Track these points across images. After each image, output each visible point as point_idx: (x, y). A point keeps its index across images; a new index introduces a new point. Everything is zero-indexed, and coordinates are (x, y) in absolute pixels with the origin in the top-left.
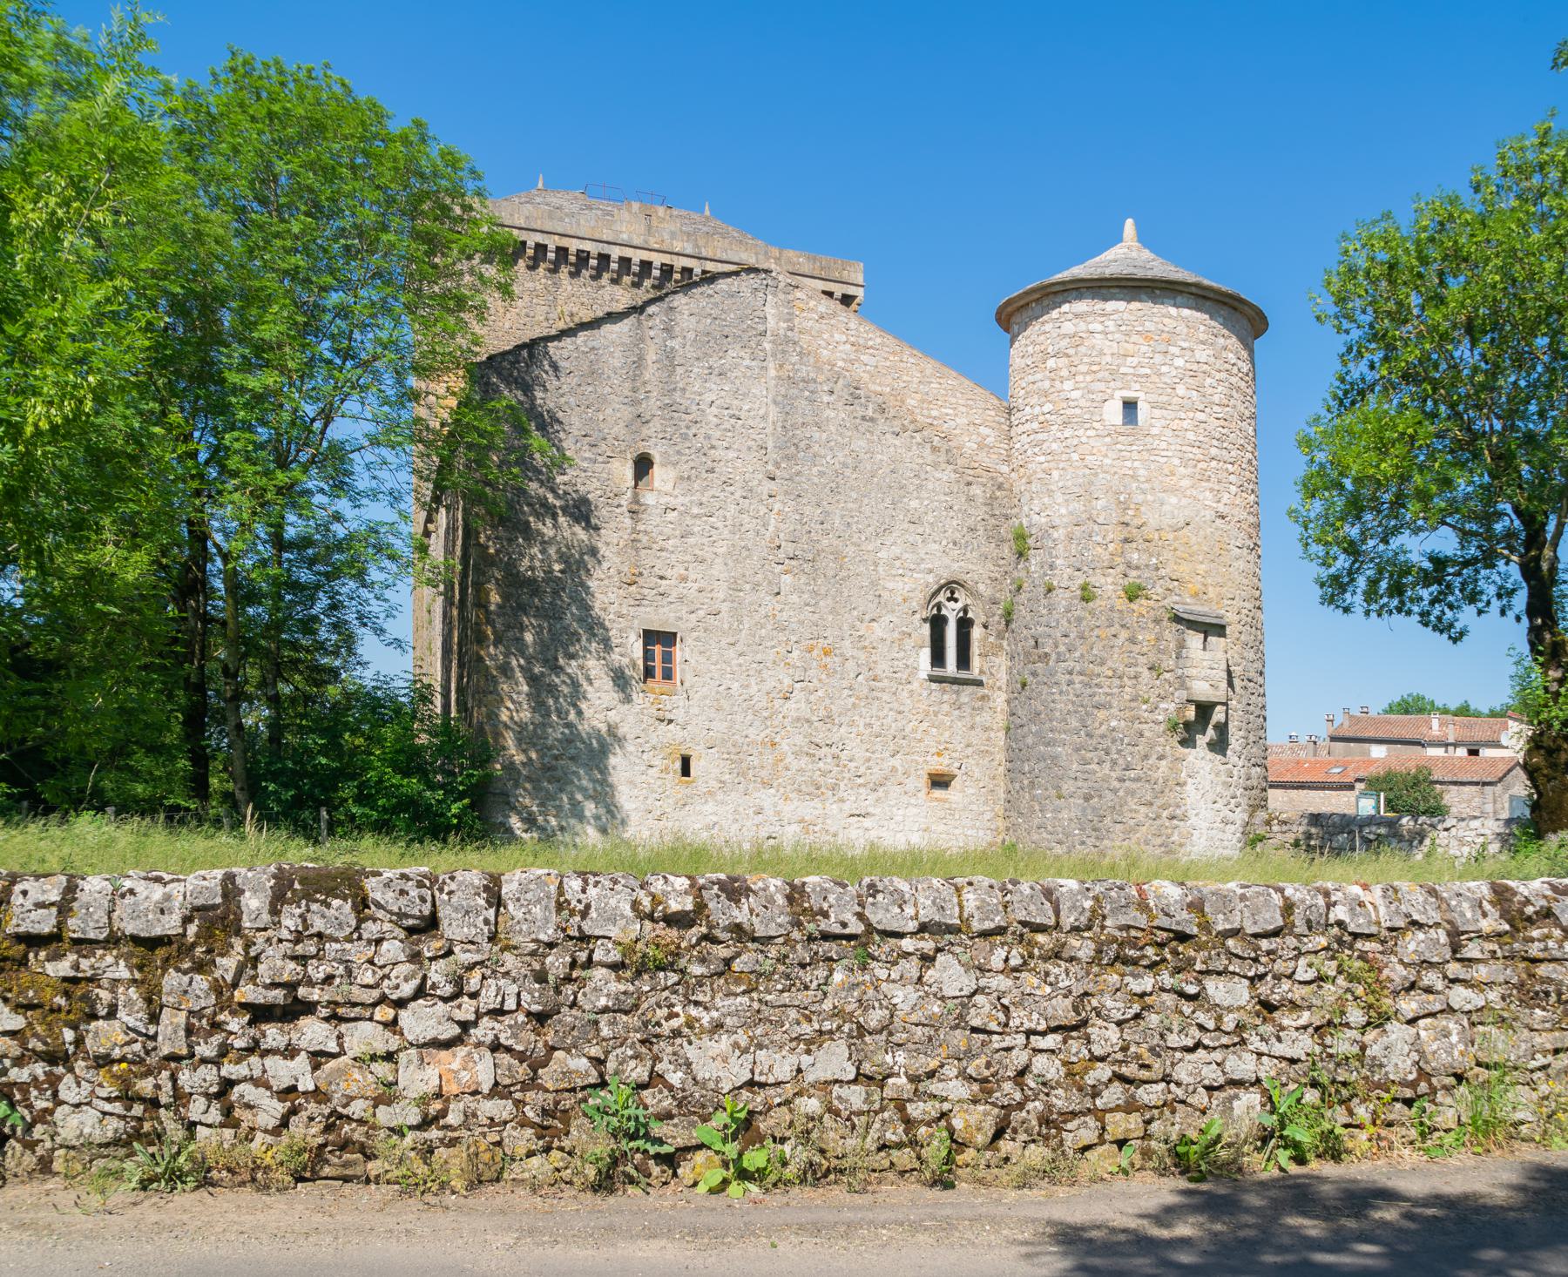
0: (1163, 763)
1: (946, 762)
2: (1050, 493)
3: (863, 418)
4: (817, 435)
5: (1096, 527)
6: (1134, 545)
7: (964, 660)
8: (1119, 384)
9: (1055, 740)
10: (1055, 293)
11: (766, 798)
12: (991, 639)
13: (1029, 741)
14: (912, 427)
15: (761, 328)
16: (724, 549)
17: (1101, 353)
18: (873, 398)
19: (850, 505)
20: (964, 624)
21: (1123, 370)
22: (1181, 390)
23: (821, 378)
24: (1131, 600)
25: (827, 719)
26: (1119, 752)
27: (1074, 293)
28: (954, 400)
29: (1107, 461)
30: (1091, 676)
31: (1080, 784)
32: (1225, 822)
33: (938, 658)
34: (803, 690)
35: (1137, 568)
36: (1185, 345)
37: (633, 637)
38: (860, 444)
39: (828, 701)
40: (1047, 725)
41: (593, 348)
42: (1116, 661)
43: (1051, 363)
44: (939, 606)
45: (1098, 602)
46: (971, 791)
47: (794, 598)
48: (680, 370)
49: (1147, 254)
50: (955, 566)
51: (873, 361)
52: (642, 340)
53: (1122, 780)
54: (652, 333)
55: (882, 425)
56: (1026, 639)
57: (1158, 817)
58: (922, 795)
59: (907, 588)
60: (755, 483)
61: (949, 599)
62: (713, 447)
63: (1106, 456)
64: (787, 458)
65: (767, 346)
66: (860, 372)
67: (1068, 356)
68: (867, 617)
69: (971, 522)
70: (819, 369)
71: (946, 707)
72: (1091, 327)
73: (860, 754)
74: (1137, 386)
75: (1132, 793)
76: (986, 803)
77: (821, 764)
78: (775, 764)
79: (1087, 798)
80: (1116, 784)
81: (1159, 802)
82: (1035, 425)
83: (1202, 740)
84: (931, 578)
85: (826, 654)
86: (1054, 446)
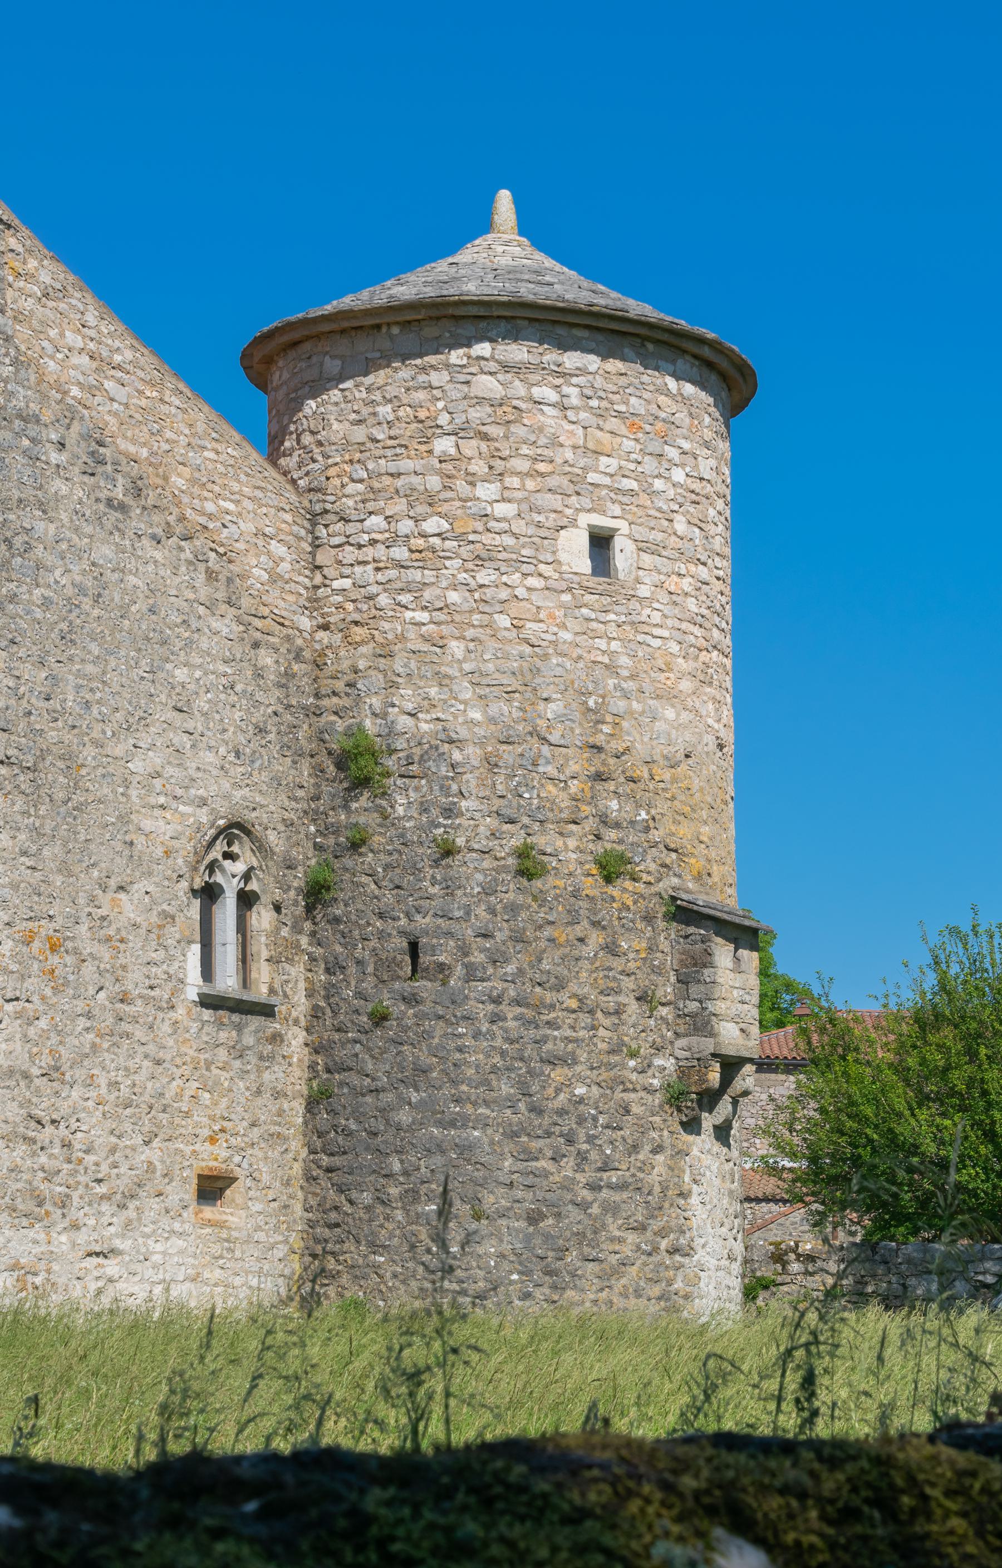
0: (660, 1158)
1: (224, 1154)
2: (442, 680)
4: (40, 526)
5: (545, 749)
6: (611, 786)
12: (285, 932)
13: (404, 1117)
14: (178, 530)
17: (555, 443)
19: (90, 669)
21: (592, 477)
22: (680, 526)
23: (47, 417)
24: (608, 879)
25: (53, 1073)
26: (590, 1139)
28: (236, 487)
29: (567, 636)
30: (539, 1007)
31: (519, 1194)
33: (207, 971)
34: (18, 1015)
35: (617, 825)
36: (686, 445)
38: (104, 552)
39: (54, 1039)
42: (583, 984)
43: (444, 445)
45: (551, 880)
46: (257, 1207)
50: (238, 794)
53: (594, 1187)
55: (136, 522)
56: (382, 936)
57: (656, 1249)
59: (170, 830)
61: (228, 856)
63: (563, 626)
66: (106, 414)
67: (485, 437)
68: (113, 883)
69: (257, 717)
70: (45, 397)
71: (222, 1054)
72: (537, 392)
73: (103, 1140)
74: (617, 510)
75: (612, 1209)
76: (276, 1229)
77: (43, 1159)
79: (534, 1218)
80: (586, 1194)
81: (655, 1225)
82: (400, 553)
83: (708, 1121)
85: (53, 949)
86: (453, 597)
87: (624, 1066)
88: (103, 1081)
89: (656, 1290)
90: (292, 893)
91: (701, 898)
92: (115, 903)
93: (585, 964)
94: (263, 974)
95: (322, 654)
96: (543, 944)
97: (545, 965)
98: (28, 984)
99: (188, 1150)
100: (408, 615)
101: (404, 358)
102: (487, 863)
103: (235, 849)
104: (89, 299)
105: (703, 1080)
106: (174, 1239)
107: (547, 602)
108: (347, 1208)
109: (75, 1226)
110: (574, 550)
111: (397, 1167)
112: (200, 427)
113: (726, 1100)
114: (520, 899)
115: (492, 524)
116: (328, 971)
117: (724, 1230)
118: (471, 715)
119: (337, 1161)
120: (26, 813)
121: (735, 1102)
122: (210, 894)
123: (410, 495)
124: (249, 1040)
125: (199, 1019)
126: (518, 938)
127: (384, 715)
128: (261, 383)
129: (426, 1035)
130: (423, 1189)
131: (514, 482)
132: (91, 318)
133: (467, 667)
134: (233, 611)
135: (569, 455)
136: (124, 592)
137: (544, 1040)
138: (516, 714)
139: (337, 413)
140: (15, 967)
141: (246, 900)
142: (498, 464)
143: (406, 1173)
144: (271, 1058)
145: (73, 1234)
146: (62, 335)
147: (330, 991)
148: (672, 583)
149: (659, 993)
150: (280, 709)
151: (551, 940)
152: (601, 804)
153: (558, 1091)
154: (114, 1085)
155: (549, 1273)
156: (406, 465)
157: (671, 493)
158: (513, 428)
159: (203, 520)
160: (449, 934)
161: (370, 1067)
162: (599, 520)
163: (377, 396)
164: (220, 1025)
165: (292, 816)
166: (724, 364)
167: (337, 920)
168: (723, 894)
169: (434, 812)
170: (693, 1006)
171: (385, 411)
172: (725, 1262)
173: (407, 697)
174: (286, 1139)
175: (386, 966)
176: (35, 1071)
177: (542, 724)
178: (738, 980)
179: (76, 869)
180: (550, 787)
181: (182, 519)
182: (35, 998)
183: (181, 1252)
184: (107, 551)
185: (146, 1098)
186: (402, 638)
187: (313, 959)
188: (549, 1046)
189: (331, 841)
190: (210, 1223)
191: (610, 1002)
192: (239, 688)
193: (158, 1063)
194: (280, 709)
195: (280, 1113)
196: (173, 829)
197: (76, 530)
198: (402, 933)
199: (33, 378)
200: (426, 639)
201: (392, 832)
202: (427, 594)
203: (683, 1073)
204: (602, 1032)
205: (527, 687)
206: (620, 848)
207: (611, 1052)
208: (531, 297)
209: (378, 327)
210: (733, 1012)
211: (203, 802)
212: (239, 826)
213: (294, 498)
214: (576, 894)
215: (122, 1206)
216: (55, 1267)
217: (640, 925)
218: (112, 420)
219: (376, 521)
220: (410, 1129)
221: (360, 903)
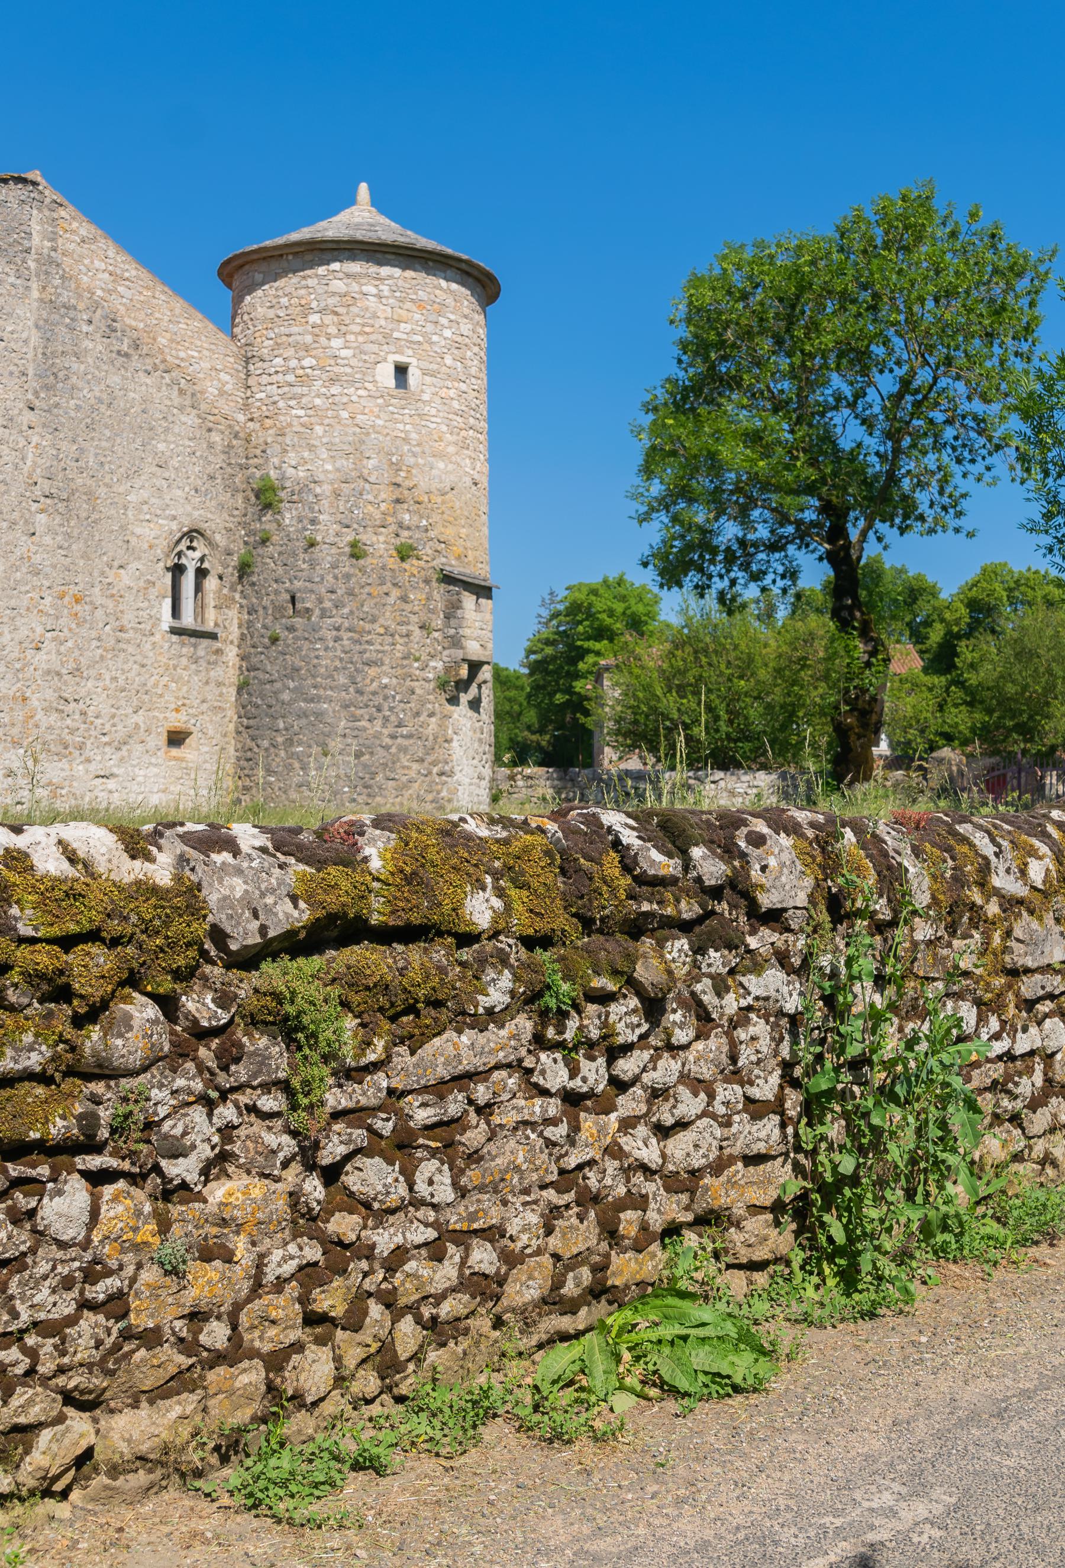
0: (433, 720)
1: (185, 718)
2: (311, 448)
3: (119, 353)
4: (75, 366)
5: (367, 486)
6: (405, 506)
8: (393, 348)
9: (319, 697)
10: (322, 250)
12: (225, 591)
13: (286, 696)
14: (162, 367)
17: (375, 316)
18: (128, 333)
19: (104, 444)
21: (396, 335)
22: (448, 360)
23: (81, 306)
24: (403, 559)
26: (391, 709)
27: (347, 253)
28: (199, 343)
30: (362, 632)
31: (349, 741)
33: (176, 612)
34: (54, 639)
35: (409, 528)
36: (452, 317)
38: (115, 380)
39: (77, 653)
40: (309, 682)
42: (387, 619)
43: (315, 318)
45: (369, 560)
46: (206, 749)
47: (48, 540)
49: (383, 220)
50: (196, 513)
51: (128, 294)
53: (393, 737)
55: (135, 362)
56: (277, 592)
57: (430, 773)
59: (153, 534)
60: (16, 412)
61: (189, 548)
63: (378, 417)
64: (47, 387)
65: (32, 265)
66: (118, 305)
67: (336, 314)
68: (116, 564)
69: (210, 470)
70: (80, 296)
71: (184, 661)
72: (365, 289)
73: (106, 710)
74: (410, 352)
75: (403, 749)
77: (69, 721)
78: (26, 721)
79: (358, 755)
80: (388, 741)
81: (430, 759)
82: (290, 378)
83: (464, 698)
84: (174, 526)
85: (77, 601)
87: (411, 666)
88: (107, 677)
89: (430, 797)
90: (230, 569)
91: (456, 569)
92: (117, 575)
93: (389, 608)
94: (211, 615)
95: (250, 435)
96: (364, 596)
97: (366, 609)
98: (61, 621)
99: (161, 716)
100: (294, 412)
101: (295, 272)
102: (334, 551)
103: (195, 544)
104: (110, 243)
105: (457, 674)
106: (151, 768)
107: (370, 404)
108: (256, 750)
109: (88, 761)
110: (386, 375)
111: (281, 725)
112: (177, 311)
113: (474, 685)
114: (352, 571)
115: (339, 361)
116: (249, 613)
117: (475, 762)
118: (326, 467)
119: (251, 722)
120: (62, 525)
121: (479, 687)
122: (178, 570)
123: (296, 346)
124: (201, 652)
125: (169, 641)
126: (351, 593)
127: (280, 468)
128: (229, 286)
129: (300, 649)
130: (295, 738)
131: (351, 338)
132: (111, 253)
133: (325, 440)
134: (195, 411)
135: (383, 322)
136: (127, 401)
137: (364, 652)
138: (351, 466)
139: (261, 302)
140: (52, 612)
141: (201, 573)
142: (343, 328)
143: (286, 729)
144: (215, 663)
145: (87, 765)
146: (92, 262)
147: (250, 624)
148: (443, 393)
149: (433, 624)
150: (224, 465)
151: (369, 594)
152: (399, 516)
153: (372, 681)
154: (115, 679)
155: (366, 787)
156: (295, 329)
157: (443, 343)
158: (351, 308)
159: (177, 362)
160: (312, 591)
161: (269, 668)
162: (402, 359)
163: (280, 293)
164: (183, 644)
165: (231, 525)
166: (476, 273)
167: (253, 584)
168: (479, 570)
169: (305, 522)
170: (452, 631)
171: (284, 301)
172: (476, 781)
173: (292, 458)
174: (224, 710)
175: (279, 609)
176: (64, 671)
177: (366, 472)
178: (479, 616)
179: (93, 556)
180: (370, 507)
181: (164, 361)
182: (65, 630)
183: (156, 775)
184: (117, 379)
185: (135, 686)
186: (290, 425)
187: (241, 607)
188: (367, 655)
189: (252, 539)
190: (175, 759)
191: (404, 629)
192: (198, 454)
193: (143, 666)
194: (224, 465)
195: (221, 695)
196: (155, 534)
198: (287, 591)
199: (73, 286)
200: (303, 425)
201: (283, 534)
202: (304, 400)
203: (447, 670)
204: (398, 647)
205: (357, 451)
206: (410, 541)
207: (404, 658)
208: (361, 238)
209: (281, 255)
210: (475, 635)
211: (174, 518)
212: (196, 531)
213: (235, 349)
214: (383, 568)
215: (119, 749)
216: (75, 784)
217: (422, 585)
218: (121, 308)
219: (278, 361)
220: (289, 704)
221: (260, 576)
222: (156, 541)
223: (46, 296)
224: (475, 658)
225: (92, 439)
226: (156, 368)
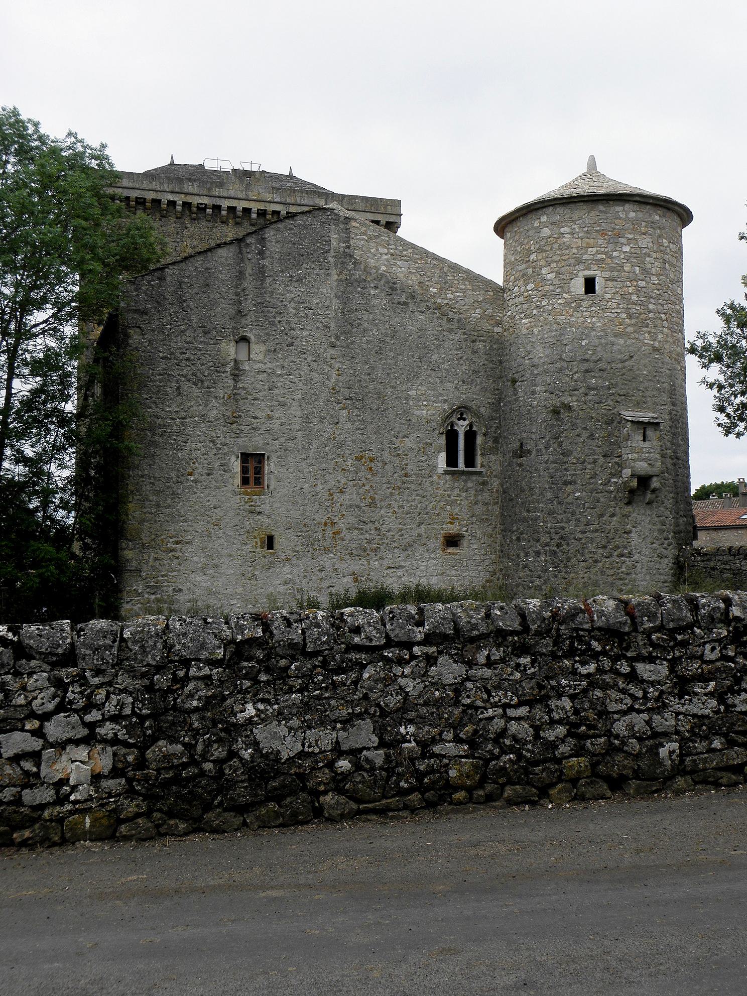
3: (399, 303)
7: (470, 461)
8: (582, 267)
11: (327, 560)
12: (490, 444)
15: (327, 248)
16: (300, 396)
20: (471, 436)
28: (463, 287)
29: (574, 319)
32: (661, 556)
33: (452, 460)
35: (594, 389)
37: (233, 459)
41: (207, 269)
44: (452, 425)
47: (349, 425)
48: (268, 280)
52: (242, 260)
54: (249, 256)
55: (412, 307)
57: (611, 555)
58: (439, 552)
61: (459, 419)
62: (292, 329)
63: (572, 316)
64: (344, 333)
65: (331, 260)
71: (457, 491)
72: (562, 230)
84: (446, 406)
87: (596, 483)
98: (360, 474)
109: (381, 558)
110: (578, 286)
128: (502, 237)
157: (622, 256)
176: (363, 505)
181: (435, 303)
194: (486, 362)
197: (383, 315)
204: (587, 471)
211: (446, 401)
222: (432, 418)
223: (343, 277)
224: (643, 473)
225: (381, 359)
226: (428, 308)
